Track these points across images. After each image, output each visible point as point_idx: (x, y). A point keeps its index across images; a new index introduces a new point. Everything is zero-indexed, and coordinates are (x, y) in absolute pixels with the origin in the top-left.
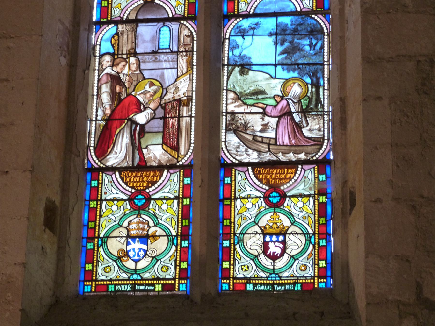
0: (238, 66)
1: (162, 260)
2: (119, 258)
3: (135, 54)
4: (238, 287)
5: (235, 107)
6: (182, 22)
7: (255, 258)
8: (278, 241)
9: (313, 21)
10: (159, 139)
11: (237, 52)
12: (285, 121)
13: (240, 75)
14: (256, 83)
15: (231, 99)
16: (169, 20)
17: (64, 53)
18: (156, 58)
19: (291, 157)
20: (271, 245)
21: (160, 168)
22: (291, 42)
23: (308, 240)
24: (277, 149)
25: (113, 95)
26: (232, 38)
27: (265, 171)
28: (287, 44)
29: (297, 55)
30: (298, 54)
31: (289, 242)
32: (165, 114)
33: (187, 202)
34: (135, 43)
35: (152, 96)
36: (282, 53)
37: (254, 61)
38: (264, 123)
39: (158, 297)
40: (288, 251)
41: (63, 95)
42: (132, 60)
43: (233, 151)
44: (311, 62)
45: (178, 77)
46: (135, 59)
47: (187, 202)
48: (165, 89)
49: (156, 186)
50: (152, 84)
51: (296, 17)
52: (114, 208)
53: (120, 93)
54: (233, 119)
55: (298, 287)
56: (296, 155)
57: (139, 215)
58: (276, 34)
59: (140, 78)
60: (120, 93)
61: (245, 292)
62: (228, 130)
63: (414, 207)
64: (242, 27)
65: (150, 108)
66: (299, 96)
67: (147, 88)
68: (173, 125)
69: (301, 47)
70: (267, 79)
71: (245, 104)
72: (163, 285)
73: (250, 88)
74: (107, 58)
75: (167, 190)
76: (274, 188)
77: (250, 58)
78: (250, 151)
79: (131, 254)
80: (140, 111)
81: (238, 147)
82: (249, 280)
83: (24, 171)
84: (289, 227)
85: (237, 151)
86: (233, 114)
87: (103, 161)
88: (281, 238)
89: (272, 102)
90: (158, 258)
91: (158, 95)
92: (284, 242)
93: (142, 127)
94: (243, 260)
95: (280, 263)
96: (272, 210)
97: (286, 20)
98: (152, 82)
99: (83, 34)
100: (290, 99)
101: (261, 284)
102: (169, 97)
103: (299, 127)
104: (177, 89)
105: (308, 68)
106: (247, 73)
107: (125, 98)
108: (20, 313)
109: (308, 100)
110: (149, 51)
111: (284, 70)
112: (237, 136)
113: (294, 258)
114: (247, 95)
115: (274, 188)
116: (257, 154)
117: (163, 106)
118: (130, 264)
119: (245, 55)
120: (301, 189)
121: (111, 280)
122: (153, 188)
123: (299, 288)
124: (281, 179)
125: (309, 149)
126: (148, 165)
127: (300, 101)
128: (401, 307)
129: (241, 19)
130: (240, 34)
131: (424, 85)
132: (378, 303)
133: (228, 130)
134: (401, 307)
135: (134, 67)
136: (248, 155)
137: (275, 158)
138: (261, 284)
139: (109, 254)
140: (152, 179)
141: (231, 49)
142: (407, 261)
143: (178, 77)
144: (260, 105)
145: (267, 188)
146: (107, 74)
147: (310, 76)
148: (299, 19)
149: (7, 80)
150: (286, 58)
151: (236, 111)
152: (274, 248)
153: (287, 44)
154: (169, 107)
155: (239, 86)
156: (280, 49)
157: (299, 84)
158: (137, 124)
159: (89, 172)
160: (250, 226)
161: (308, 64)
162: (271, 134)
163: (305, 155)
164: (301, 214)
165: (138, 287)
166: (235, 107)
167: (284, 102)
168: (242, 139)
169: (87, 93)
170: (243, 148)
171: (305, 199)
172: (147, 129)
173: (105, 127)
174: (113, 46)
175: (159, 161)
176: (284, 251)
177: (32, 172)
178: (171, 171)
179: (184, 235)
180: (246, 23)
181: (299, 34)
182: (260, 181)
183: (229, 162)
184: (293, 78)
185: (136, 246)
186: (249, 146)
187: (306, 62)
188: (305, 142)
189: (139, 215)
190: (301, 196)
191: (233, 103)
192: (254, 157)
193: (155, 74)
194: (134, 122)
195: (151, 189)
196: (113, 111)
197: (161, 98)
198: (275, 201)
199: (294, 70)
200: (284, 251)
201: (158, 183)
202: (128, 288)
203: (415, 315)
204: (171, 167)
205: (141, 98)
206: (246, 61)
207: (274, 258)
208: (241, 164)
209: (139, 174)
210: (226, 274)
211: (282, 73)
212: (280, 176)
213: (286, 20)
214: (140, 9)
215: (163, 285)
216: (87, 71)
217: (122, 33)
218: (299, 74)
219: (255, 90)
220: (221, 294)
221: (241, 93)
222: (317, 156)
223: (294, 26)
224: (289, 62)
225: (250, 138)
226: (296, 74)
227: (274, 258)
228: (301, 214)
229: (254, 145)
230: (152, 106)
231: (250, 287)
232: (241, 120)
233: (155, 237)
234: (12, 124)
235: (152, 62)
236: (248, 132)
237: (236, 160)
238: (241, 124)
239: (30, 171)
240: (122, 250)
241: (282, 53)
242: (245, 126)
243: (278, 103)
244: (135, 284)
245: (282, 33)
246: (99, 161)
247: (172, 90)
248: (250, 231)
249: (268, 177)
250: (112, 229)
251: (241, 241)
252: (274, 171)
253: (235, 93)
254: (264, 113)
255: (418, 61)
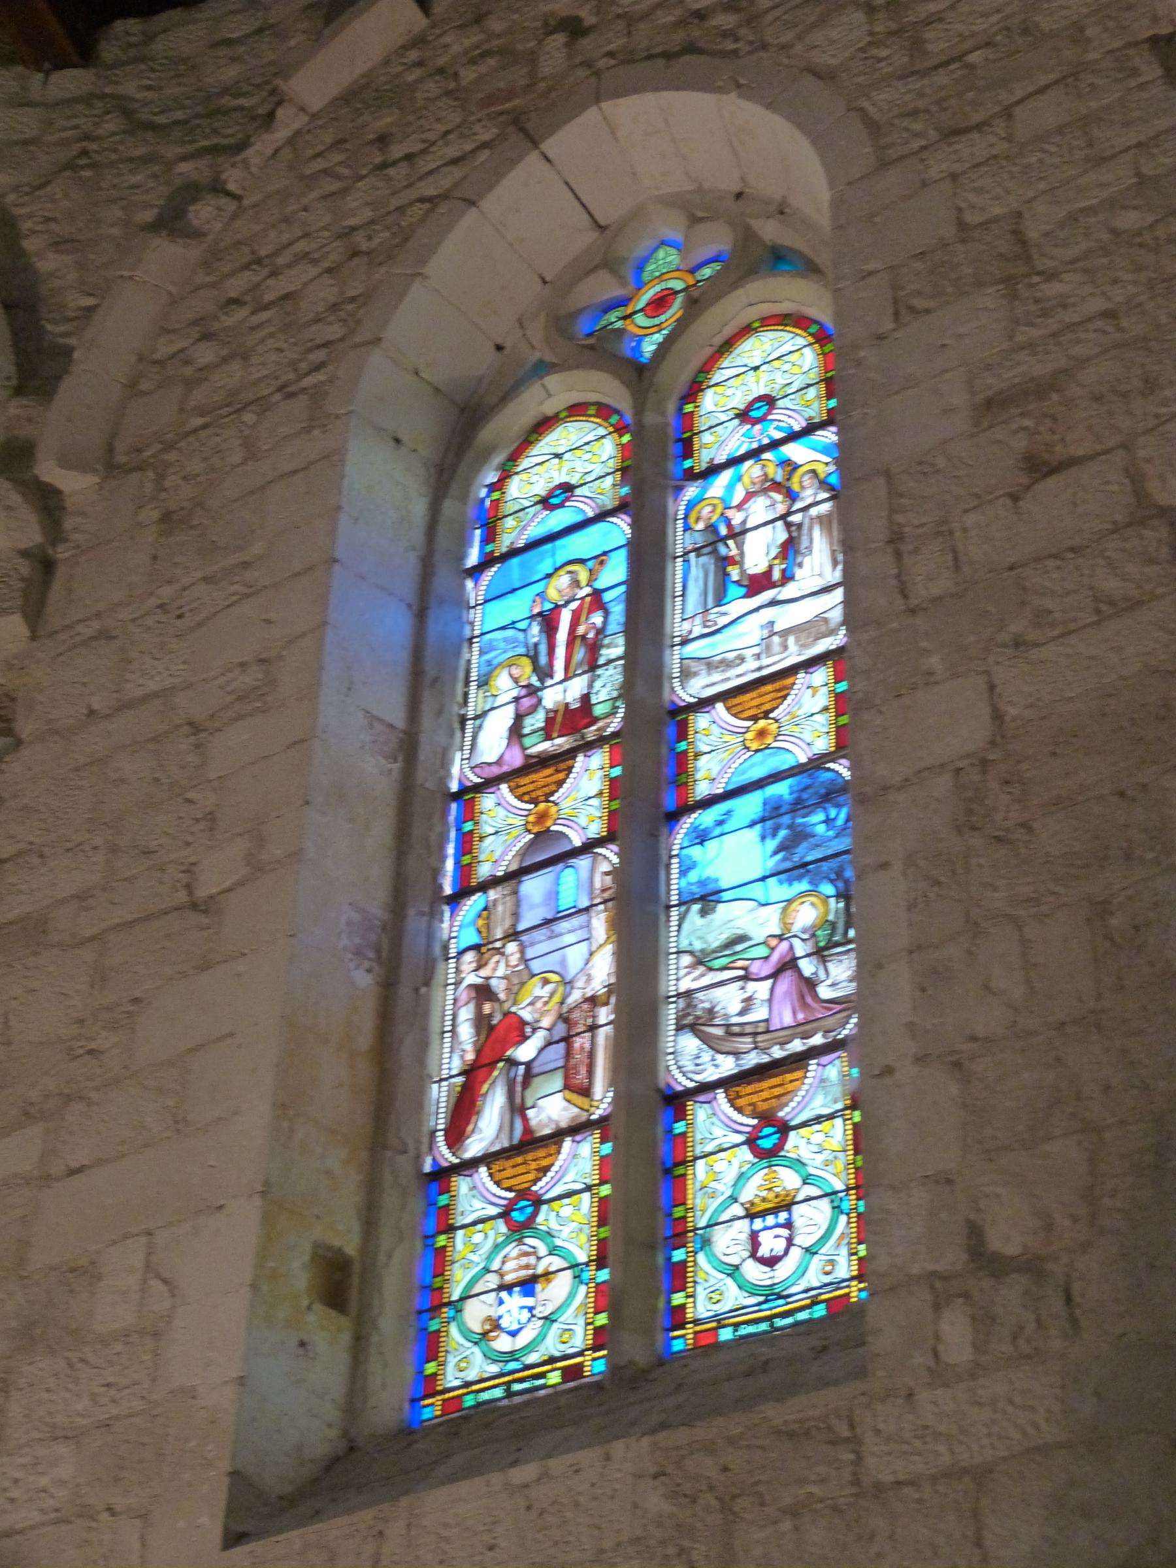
0: (695, 901)
1: (560, 1320)
2: (485, 1334)
3: (513, 935)
4: (706, 1340)
5: (694, 980)
6: (595, 851)
7: (734, 1271)
8: (778, 1226)
9: (829, 775)
10: (557, 1082)
11: (693, 876)
12: (786, 982)
13: (702, 916)
14: (730, 925)
15: (686, 967)
16: (576, 852)
17: (367, 964)
18: (552, 931)
19: (797, 1046)
20: (764, 1237)
21: (559, 1135)
22: (791, 827)
23: (837, 1209)
24: (768, 1040)
25: (481, 1022)
26: (684, 852)
27: (750, 1089)
28: (783, 833)
29: (802, 849)
30: (804, 845)
31: (798, 1222)
32: (569, 1030)
33: (606, 1190)
34: (516, 915)
35: (546, 1003)
36: (775, 853)
37: (723, 885)
38: (746, 995)
39: (556, 1393)
40: (797, 1240)
41: (365, 1041)
42: (512, 947)
43: (689, 1066)
44: (830, 852)
45: (591, 954)
46: (517, 943)
47: (606, 1190)
48: (568, 984)
49: (550, 1174)
50: (546, 982)
51: (798, 778)
52: (478, 1238)
53: (490, 1016)
54: (689, 1005)
55: (820, 1311)
56: (805, 1041)
57: (520, 1241)
58: (763, 820)
59: (525, 976)
60: (490, 1016)
61: (718, 1346)
62: (680, 1028)
63: (957, 1065)
64: (701, 827)
65: (540, 1028)
66: (813, 926)
67: (538, 992)
68: (582, 1048)
69: (809, 829)
70: (752, 910)
71: (711, 969)
72: (565, 1370)
73: (720, 937)
74: (470, 957)
75: (569, 1177)
76: (767, 1118)
77: (717, 880)
78: (720, 1057)
79: (504, 1323)
80: (524, 1038)
81: (713, 1060)
82: (720, 1321)
83: (251, 1196)
84: (798, 1190)
85: (697, 1065)
86: (689, 994)
87: (458, 1153)
88: (783, 1216)
89: (762, 951)
90: (554, 1317)
91: (557, 998)
92: (789, 1225)
93: (528, 1065)
94: (712, 1282)
95: (783, 1270)
96: (764, 1163)
97: (782, 789)
98: (544, 978)
99: (415, 923)
100: (795, 936)
101: (748, 1323)
102: (576, 996)
103: (810, 984)
104: (589, 978)
105: (825, 866)
106: (713, 910)
107: (500, 1021)
108: (226, 1481)
109: (829, 927)
110: (577, 927)
111: (781, 882)
112: (698, 1036)
113: (810, 1251)
114: (714, 951)
115: (767, 1118)
116: (734, 1059)
117: (564, 1019)
118: (503, 1343)
119: (708, 878)
120: (820, 1105)
121: (467, 1384)
122: (545, 1180)
123: (824, 1313)
124: (778, 1097)
125: (830, 1022)
126: (538, 1134)
127: (813, 935)
128: (938, 1284)
129: (700, 812)
130: (697, 841)
131: (970, 812)
132: (891, 1289)
133: (680, 1028)
134: (938, 1284)
135: (514, 960)
136: (716, 1066)
137: (765, 1059)
138: (748, 1323)
139: (466, 1332)
140: (544, 1163)
141: (683, 873)
142: (949, 1181)
143: (591, 954)
144: (740, 964)
145: (755, 1122)
146: (470, 986)
147: (832, 881)
148: (803, 780)
149: (231, 1035)
150: (784, 859)
151: (693, 988)
152: (770, 1243)
153: (783, 833)
154: (576, 1015)
155: (700, 938)
156: (772, 844)
157: (813, 904)
158: (518, 1064)
159: (433, 1181)
160: (724, 1207)
161: (825, 859)
162: (759, 1013)
163: (824, 1036)
164: (820, 1158)
165: (517, 1387)
166: (694, 980)
167: (784, 945)
168: (705, 1039)
169: (425, 1030)
170: (707, 1056)
171: (826, 1125)
172: (536, 1070)
173: (464, 1086)
174: (479, 932)
175: (557, 1123)
176: (790, 1242)
177: (263, 1193)
178: (578, 1138)
179: (601, 1262)
180: (706, 818)
181: (805, 807)
182: (739, 1110)
183: (680, 1088)
184: (802, 894)
185: (515, 1301)
186: (719, 1048)
187: (821, 856)
188: (823, 1011)
189: (520, 1241)
190: (818, 1119)
191: (689, 973)
192: (727, 1066)
193: (550, 962)
194: (513, 1063)
195: (540, 1184)
196: (479, 1052)
197: (562, 1003)
198: (766, 1144)
199: (799, 878)
200: (790, 1242)
201: (554, 1169)
202: (498, 1393)
203: (967, 1296)
204: (576, 1129)
205: (526, 1015)
206: (712, 887)
207: (771, 1262)
208: (706, 1088)
209: (519, 1160)
210: (677, 1318)
211: (778, 890)
212: (777, 1091)
213: (782, 789)
214: (528, 848)
215: (565, 1370)
216: (423, 990)
217: (495, 901)
218: (810, 882)
219: (728, 938)
220: (665, 1359)
221: (702, 951)
222: (845, 1032)
223: (794, 796)
224: (788, 865)
225: (719, 1032)
226: (804, 886)
227: (771, 1262)
228: (820, 1158)
229: (728, 1044)
230: (546, 1022)
231: (726, 1334)
232: (704, 1001)
233: (547, 1275)
234: (235, 1114)
235: (545, 940)
236: (717, 1021)
237: (692, 1080)
238: (704, 1009)
239: (262, 1192)
240: (489, 1319)
241: (775, 853)
242: (711, 1012)
243: (773, 949)
244: (509, 1383)
245: (774, 814)
246: (454, 1154)
247: (580, 983)
248: (725, 1216)
249: (754, 1098)
250: (475, 1280)
251: (706, 1242)
252: (765, 1084)
253: (691, 953)
254: (746, 978)
255: (958, 770)
